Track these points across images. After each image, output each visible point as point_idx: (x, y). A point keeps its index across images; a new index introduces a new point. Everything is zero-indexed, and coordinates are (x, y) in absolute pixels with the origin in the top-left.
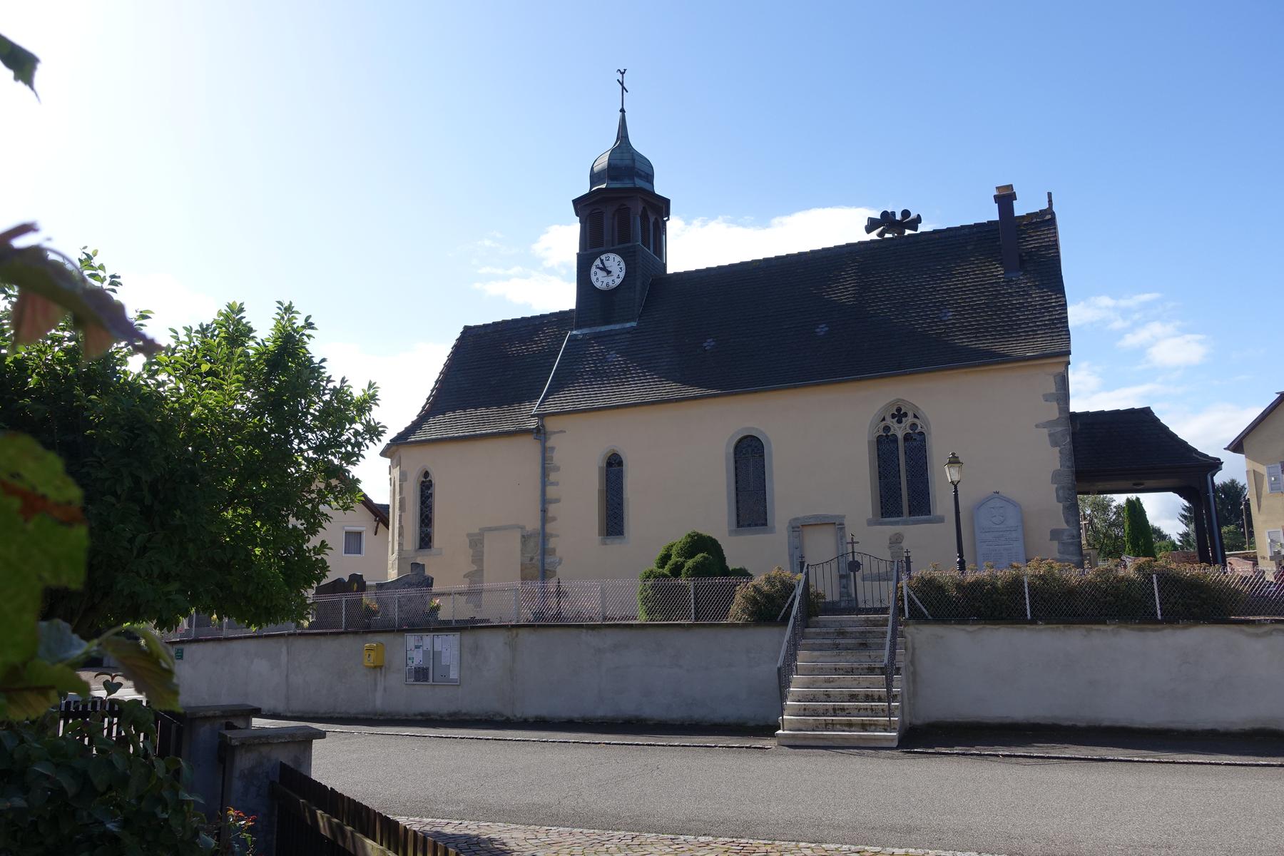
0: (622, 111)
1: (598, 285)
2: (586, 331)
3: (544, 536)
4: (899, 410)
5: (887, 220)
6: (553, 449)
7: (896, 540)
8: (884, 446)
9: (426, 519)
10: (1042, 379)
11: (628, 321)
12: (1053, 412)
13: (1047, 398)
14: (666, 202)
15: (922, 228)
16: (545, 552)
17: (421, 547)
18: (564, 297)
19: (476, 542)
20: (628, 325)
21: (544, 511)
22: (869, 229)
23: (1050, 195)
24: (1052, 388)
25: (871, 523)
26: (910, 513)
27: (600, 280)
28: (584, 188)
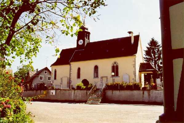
3: (70, 78)
8: (113, 67)
18: (75, 46)
19: (62, 79)
24: (134, 60)
26: (116, 76)
27: (81, 41)
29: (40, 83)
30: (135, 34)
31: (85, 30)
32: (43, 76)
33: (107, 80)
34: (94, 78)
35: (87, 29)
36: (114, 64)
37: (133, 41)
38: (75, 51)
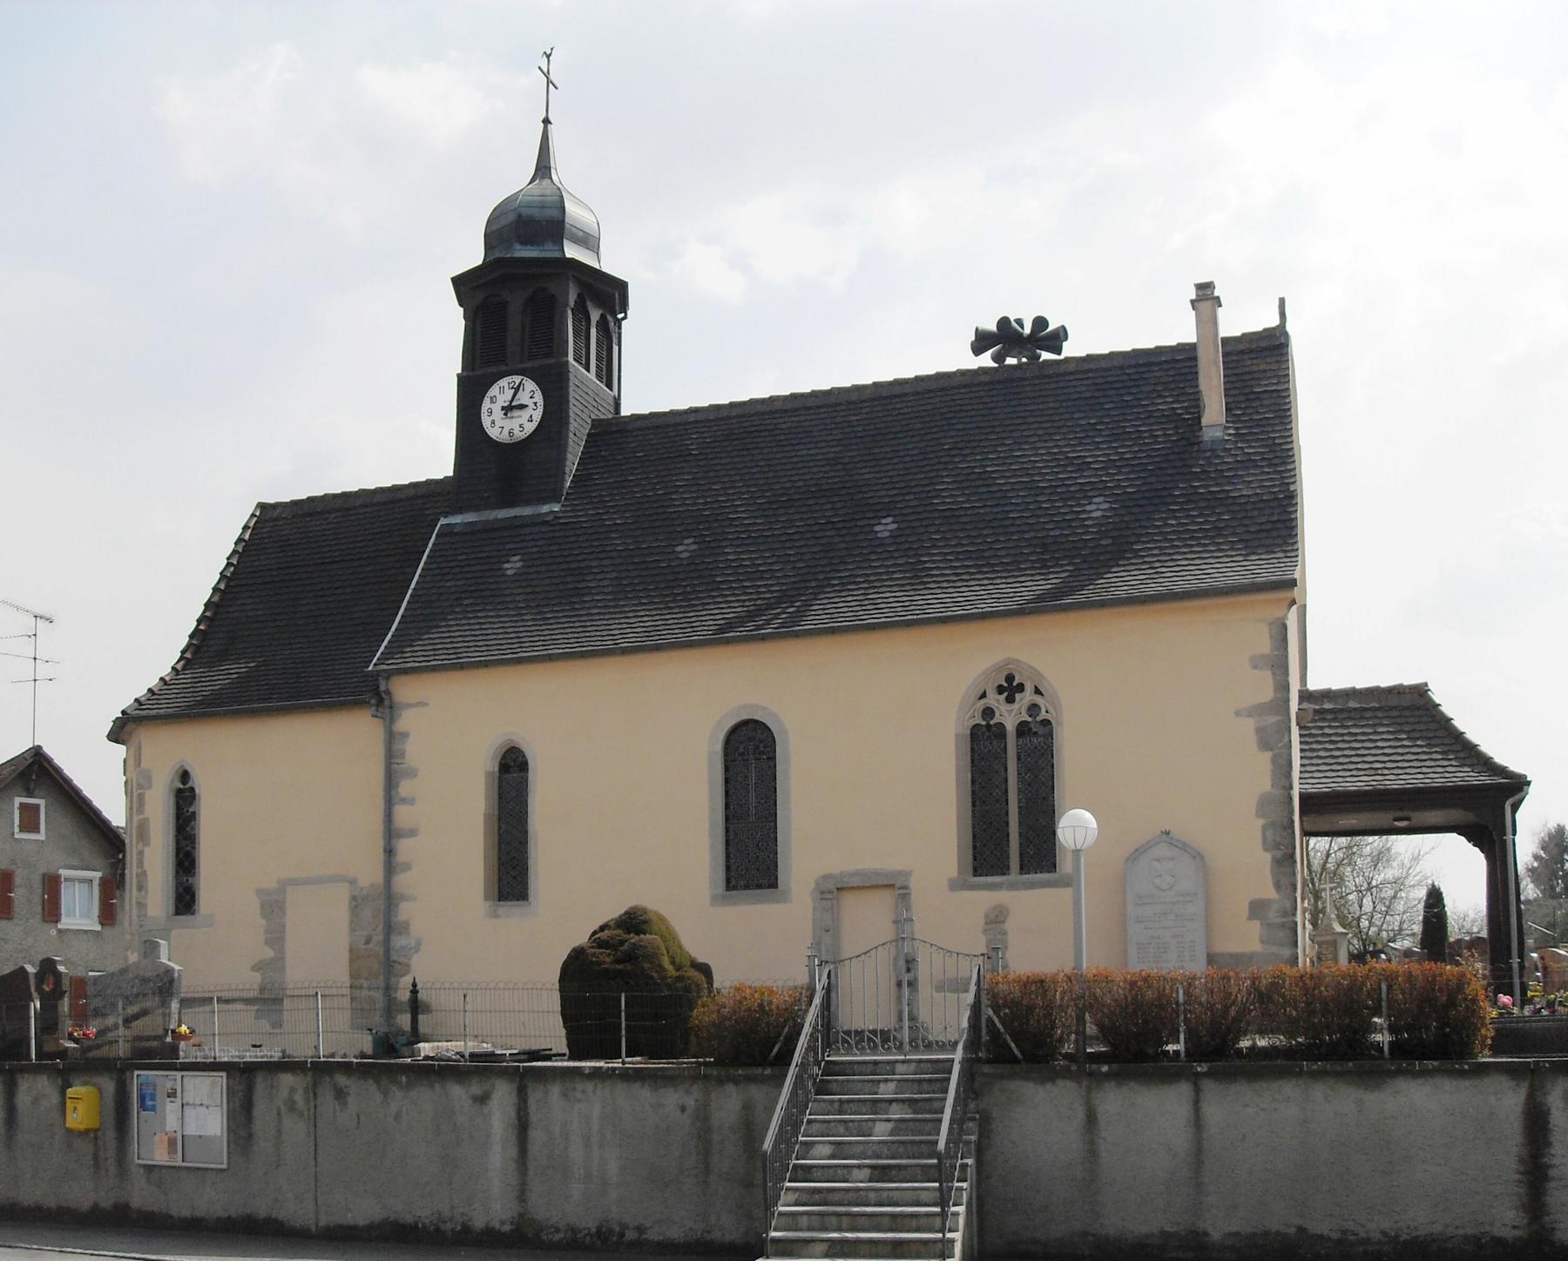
0: (546, 121)
1: (493, 433)
2: (470, 517)
3: (389, 899)
4: (1010, 678)
5: (1003, 337)
6: (405, 735)
7: (996, 919)
8: (983, 741)
9: (185, 860)
10: (1244, 628)
11: (545, 501)
12: (1264, 690)
13: (1256, 663)
14: (622, 286)
15: (1071, 349)
16: (390, 927)
17: (178, 912)
18: (430, 455)
19: (273, 906)
20: (545, 509)
21: (389, 852)
22: (978, 348)
23: (1282, 302)
24: (1265, 646)
25: (956, 885)
26: (1024, 869)
27: (499, 425)
28: (474, 257)
29: (39, 891)
30: (1236, 321)
31: (571, 251)
32: (42, 836)
33: (902, 922)
34: (715, 900)
35: (589, 241)
36: (995, 701)
37: (1214, 411)
38: (443, 521)
